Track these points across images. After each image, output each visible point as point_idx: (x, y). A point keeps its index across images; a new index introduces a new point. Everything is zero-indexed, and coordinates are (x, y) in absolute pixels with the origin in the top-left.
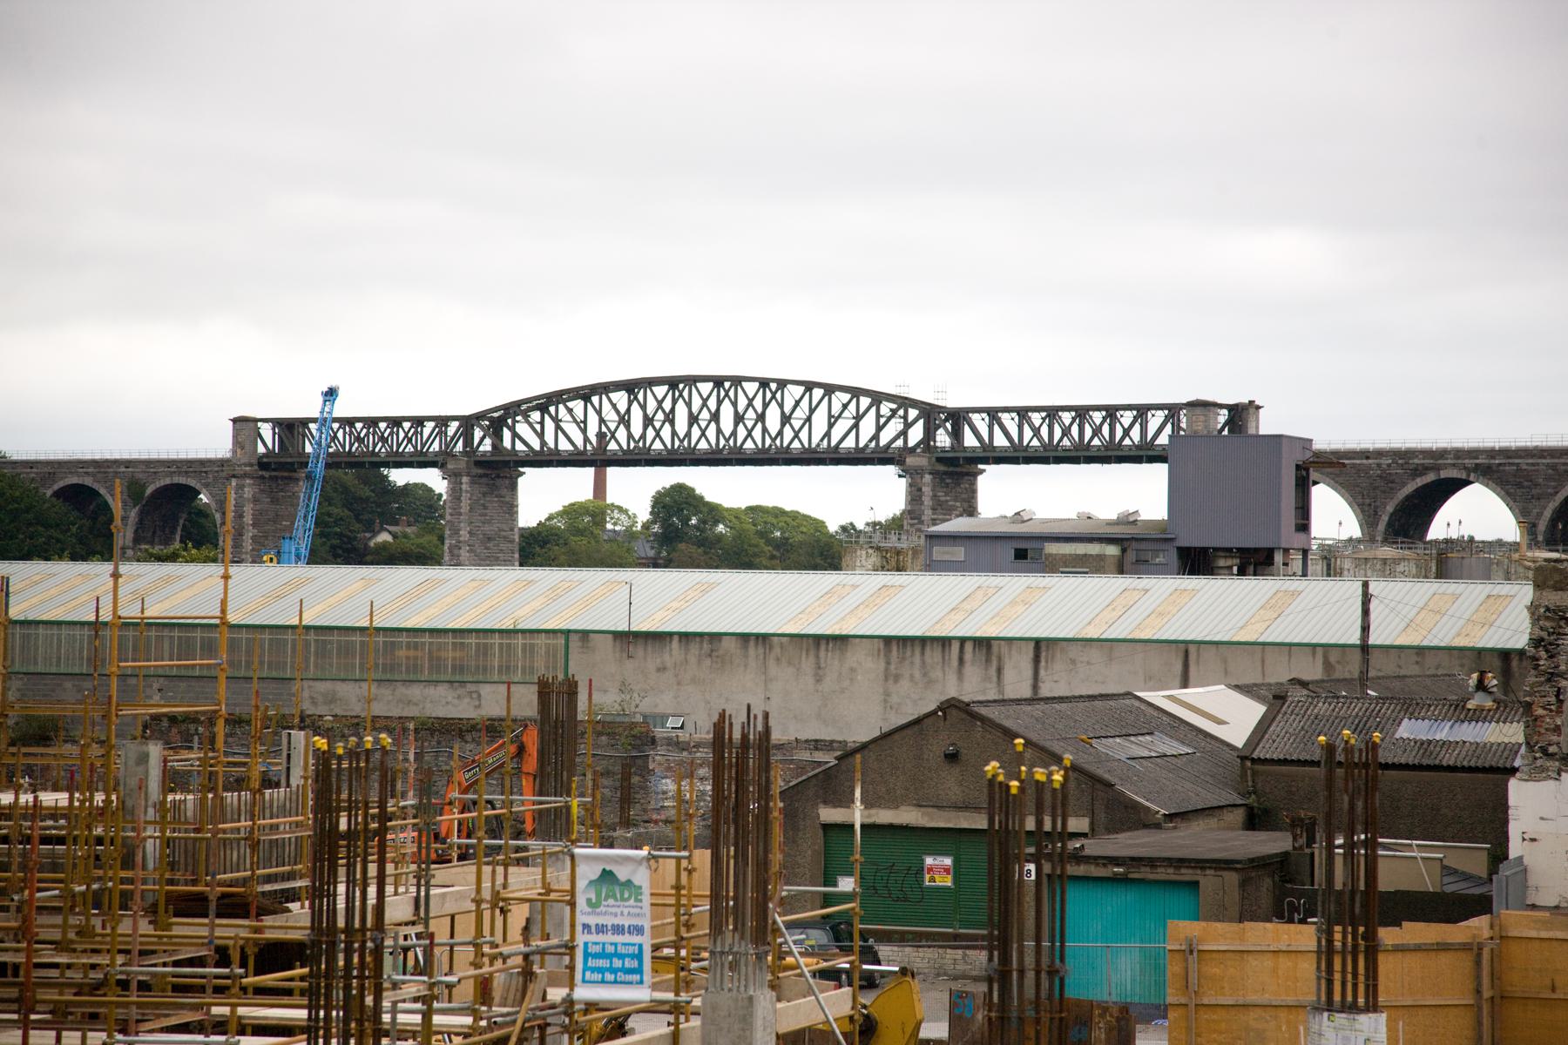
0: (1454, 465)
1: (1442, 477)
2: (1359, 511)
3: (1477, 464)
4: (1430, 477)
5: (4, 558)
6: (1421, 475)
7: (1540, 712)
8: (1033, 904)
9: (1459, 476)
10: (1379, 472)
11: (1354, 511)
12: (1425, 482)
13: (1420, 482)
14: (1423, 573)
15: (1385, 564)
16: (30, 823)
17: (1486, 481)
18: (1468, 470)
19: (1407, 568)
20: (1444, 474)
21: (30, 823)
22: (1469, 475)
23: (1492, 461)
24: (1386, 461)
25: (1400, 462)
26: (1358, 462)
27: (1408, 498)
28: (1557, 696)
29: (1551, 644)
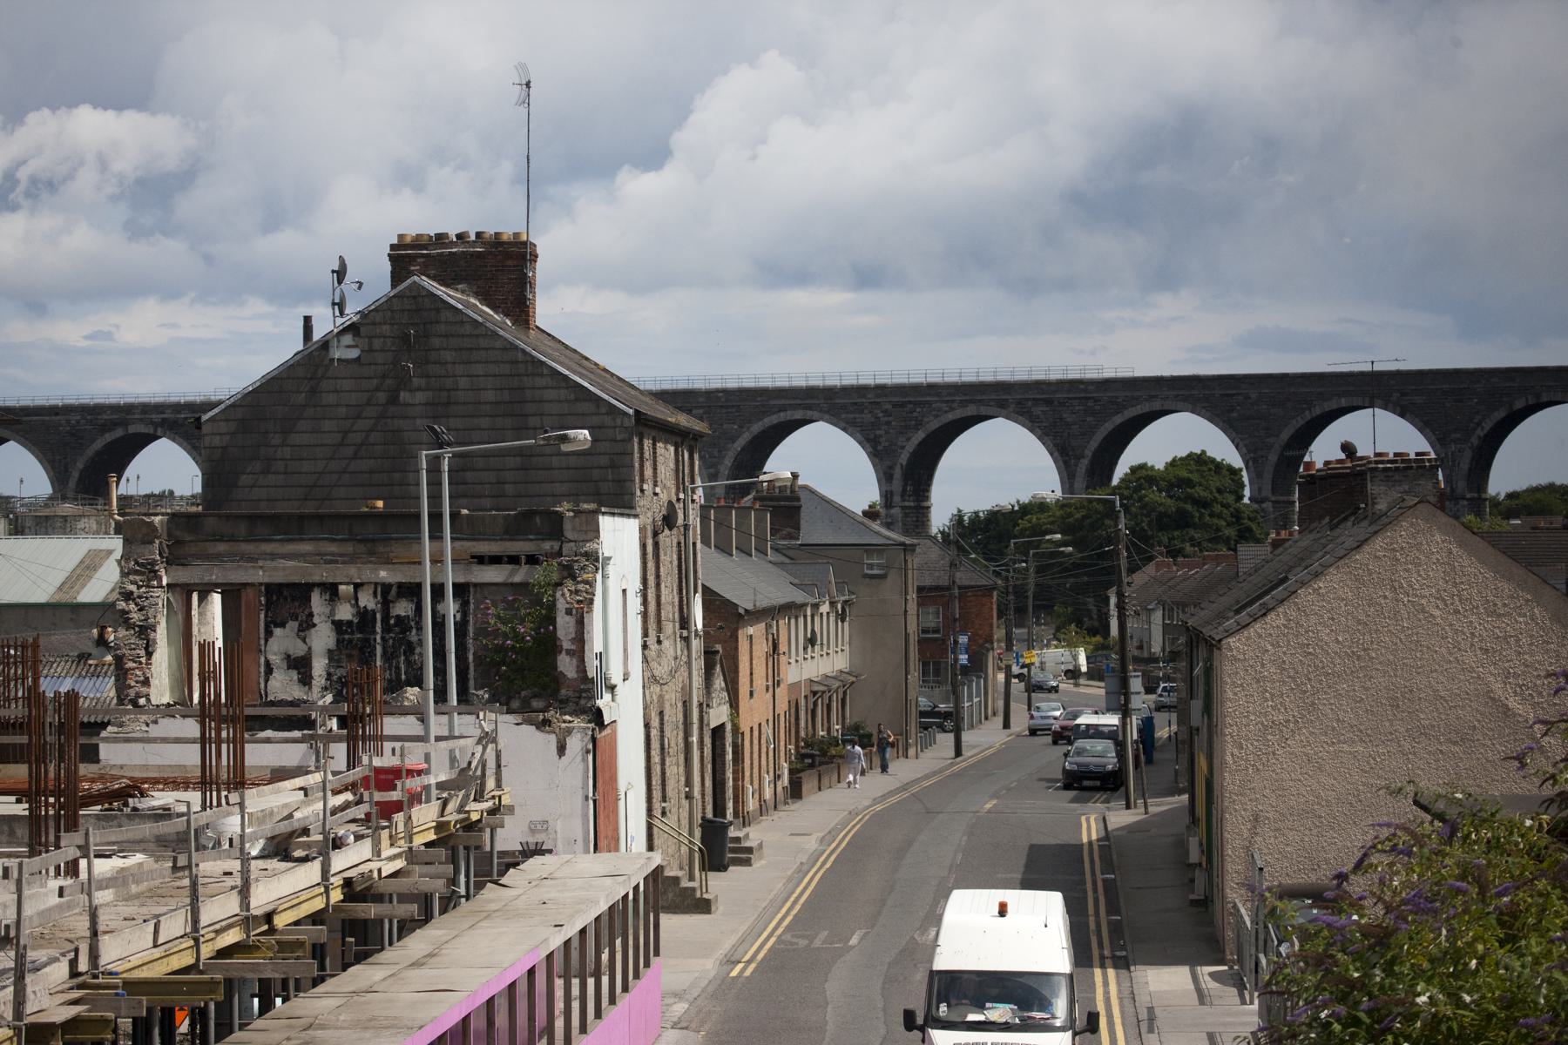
0: (141, 420)
1: (130, 432)
2: (49, 467)
3: (163, 419)
4: (119, 433)
5: (1562, 487)
6: (110, 430)
7: (131, 665)
8: (659, 788)
9: (147, 431)
10: (68, 428)
11: (44, 468)
12: (113, 438)
13: (109, 437)
14: (103, 530)
15: (66, 521)
16: (1084, 669)
17: (172, 435)
18: (156, 425)
19: (87, 526)
20: (132, 429)
21: (1084, 669)
22: (156, 430)
23: (178, 416)
24: (75, 418)
25: (89, 417)
26: (47, 418)
27: (98, 453)
28: (146, 649)
29: (140, 597)
